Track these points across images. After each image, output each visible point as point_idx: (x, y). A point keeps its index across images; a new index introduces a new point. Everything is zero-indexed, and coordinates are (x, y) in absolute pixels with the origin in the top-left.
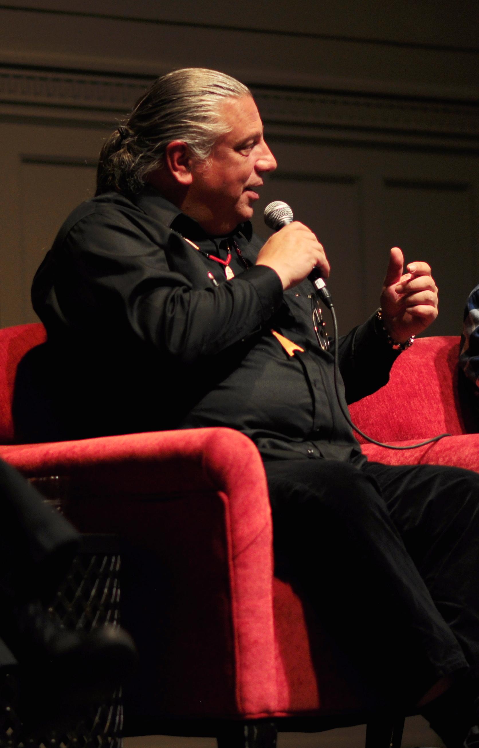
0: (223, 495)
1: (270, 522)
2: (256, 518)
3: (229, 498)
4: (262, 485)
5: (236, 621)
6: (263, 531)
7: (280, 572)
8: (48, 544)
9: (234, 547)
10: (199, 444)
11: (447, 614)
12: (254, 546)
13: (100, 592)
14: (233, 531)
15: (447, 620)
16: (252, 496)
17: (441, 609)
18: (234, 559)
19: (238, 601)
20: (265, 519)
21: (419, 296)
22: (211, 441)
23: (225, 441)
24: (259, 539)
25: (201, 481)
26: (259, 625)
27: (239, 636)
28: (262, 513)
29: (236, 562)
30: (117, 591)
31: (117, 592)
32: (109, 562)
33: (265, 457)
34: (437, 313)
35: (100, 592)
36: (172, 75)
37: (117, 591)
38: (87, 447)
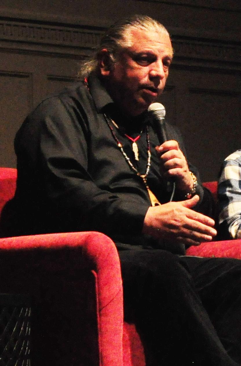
0: (93, 272)
1: (122, 290)
2: (113, 286)
3: (97, 275)
4: (119, 266)
5: (100, 348)
6: (117, 294)
7: (127, 319)
8: (170, 183)
9: (100, 304)
10: (80, 241)
11: (226, 345)
12: (112, 303)
13: (19, 329)
14: (99, 294)
15: (226, 349)
16: (112, 274)
17: (223, 342)
18: (100, 311)
19: (102, 337)
20: (119, 287)
21: (168, 154)
22: (87, 241)
23: (95, 239)
24: (115, 299)
25: (83, 261)
26: (114, 351)
27: (102, 358)
28: (118, 284)
29: (101, 312)
30: (28, 329)
31: (29, 330)
32: (24, 311)
33: (119, 249)
34: (164, 112)
35: (19, 329)
36: (112, 61)
37: (28, 329)
38: (11, 242)
